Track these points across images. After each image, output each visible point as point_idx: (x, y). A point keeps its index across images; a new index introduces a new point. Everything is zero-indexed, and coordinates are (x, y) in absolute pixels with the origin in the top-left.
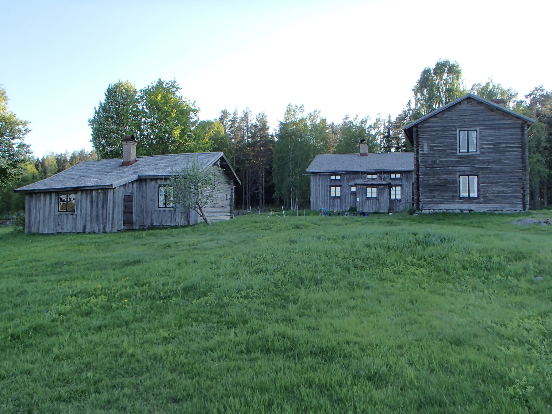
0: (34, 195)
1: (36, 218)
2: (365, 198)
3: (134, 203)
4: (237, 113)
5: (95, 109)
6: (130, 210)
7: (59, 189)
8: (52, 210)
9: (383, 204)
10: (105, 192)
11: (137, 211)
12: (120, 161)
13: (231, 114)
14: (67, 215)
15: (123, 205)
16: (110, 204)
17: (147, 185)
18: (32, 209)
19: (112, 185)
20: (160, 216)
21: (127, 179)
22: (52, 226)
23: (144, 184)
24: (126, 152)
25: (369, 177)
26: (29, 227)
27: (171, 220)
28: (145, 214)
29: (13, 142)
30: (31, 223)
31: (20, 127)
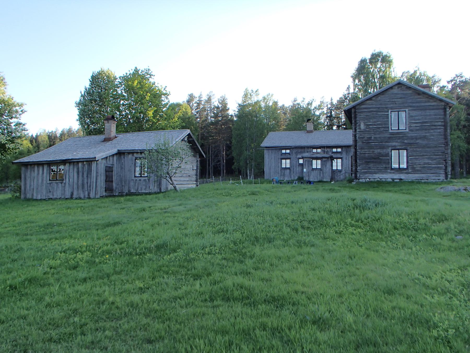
0: (29, 167)
1: (30, 186)
2: (310, 168)
3: (114, 173)
4: (202, 97)
5: (81, 93)
6: (111, 179)
7: (51, 161)
8: (45, 179)
9: (326, 174)
10: (90, 164)
11: (116, 180)
12: (102, 137)
13: (197, 98)
14: (57, 183)
15: (105, 175)
16: (94, 174)
17: (126, 158)
18: (27, 178)
19: (95, 158)
20: (136, 184)
21: (108, 152)
22: (44, 193)
23: (122, 157)
24: (107, 129)
25: (315, 151)
26: (25, 194)
27: (146, 188)
28: (123, 182)
29: (11, 121)
30: (27, 190)
31: (17, 108)
